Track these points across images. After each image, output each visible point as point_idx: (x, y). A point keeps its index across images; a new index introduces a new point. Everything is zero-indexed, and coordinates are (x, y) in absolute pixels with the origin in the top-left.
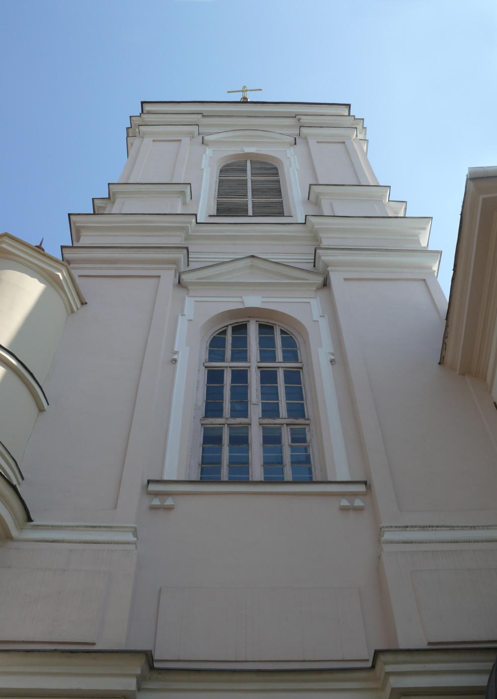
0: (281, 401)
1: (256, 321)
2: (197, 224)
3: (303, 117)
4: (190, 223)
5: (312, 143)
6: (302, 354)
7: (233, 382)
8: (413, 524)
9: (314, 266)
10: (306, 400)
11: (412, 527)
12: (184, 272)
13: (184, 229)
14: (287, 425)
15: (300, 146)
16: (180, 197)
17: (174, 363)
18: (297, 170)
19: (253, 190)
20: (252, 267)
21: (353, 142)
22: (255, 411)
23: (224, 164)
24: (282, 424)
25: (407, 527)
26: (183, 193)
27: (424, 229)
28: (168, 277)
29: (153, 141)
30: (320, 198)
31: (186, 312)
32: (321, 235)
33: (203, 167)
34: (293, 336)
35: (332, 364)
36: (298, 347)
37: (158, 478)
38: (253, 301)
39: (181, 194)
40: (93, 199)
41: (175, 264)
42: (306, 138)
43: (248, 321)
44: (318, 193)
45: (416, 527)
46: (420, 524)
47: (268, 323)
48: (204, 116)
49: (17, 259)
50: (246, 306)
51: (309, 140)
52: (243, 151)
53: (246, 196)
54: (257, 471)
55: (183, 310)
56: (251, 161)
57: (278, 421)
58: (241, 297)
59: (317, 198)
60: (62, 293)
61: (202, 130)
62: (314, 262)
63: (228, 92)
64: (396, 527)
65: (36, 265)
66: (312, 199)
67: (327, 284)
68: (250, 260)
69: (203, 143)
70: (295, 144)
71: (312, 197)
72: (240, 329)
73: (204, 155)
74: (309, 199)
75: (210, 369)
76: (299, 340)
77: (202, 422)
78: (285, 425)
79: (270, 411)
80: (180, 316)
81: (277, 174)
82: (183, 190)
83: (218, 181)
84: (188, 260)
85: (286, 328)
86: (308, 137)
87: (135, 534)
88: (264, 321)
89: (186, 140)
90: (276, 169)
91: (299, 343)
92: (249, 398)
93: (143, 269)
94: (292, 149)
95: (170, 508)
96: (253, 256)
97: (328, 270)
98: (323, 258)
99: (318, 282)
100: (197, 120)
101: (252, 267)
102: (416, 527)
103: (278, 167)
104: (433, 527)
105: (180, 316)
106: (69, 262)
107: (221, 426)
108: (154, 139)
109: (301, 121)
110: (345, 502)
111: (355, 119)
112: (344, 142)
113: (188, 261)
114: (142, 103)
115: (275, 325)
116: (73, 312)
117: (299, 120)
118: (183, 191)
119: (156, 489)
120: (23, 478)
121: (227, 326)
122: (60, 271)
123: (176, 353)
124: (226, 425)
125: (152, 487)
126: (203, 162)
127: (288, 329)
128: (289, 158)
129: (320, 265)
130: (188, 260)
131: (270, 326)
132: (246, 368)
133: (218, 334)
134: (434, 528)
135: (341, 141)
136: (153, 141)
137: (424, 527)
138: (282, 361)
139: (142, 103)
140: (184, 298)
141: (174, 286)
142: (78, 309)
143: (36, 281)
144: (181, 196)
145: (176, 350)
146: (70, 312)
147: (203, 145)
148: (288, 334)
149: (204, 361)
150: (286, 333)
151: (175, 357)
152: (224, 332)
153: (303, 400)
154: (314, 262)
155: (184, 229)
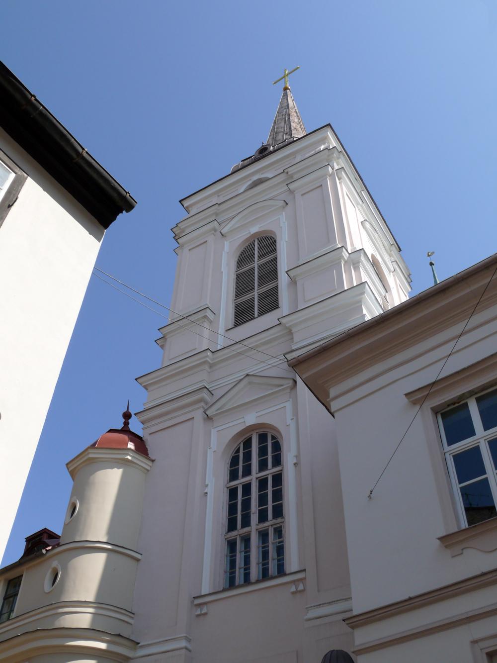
3: (289, 170)
4: (207, 356)
8: (324, 602)
11: (323, 604)
12: (207, 409)
14: (272, 525)
16: (205, 321)
18: (286, 242)
20: (250, 383)
23: (239, 253)
24: (269, 526)
25: (320, 605)
26: (205, 317)
27: (363, 293)
28: (198, 415)
30: (296, 280)
31: (212, 446)
33: (222, 270)
35: (296, 466)
37: (199, 595)
45: (325, 603)
46: (328, 601)
48: (219, 204)
54: (255, 571)
60: (134, 465)
64: (314, 606)
65: (112, 458)
68: (247, 378)
70: (287, 204)
72: (248, 443)
73: (223, 252)
78: (270, 527)
80: (209, 450)
82: (204, 315)
84: (209, 391)
85: (276, 434)
87: (188, 640)
95: (206, 614)
96: (248, 375)
99: (290, 385)
101: (250, 383)
102: (325, 603)
104: (335, 601)
105: (209, 450)
108: (190, 248)
109: (289, 173)
110: (293, 589)
116: (148, 471)
117: (287, 173)
119: (199, 602)
120: (134, 614)
122: (128, 454)
123: (207, 486)
125: (197, 601)
128: (281, 227)
130: (209, 391)
133: (235, 453)
134: (336, 602)
135: (317, 185)
137: (330, 603)
139: (180, 202)
140: (210, 431)
141: (204, 420)
142: (150, 466)
143: (116, 469)
144: (206, 320)
145: (207, 483)
152: (238, 451)
155: (205, 362)
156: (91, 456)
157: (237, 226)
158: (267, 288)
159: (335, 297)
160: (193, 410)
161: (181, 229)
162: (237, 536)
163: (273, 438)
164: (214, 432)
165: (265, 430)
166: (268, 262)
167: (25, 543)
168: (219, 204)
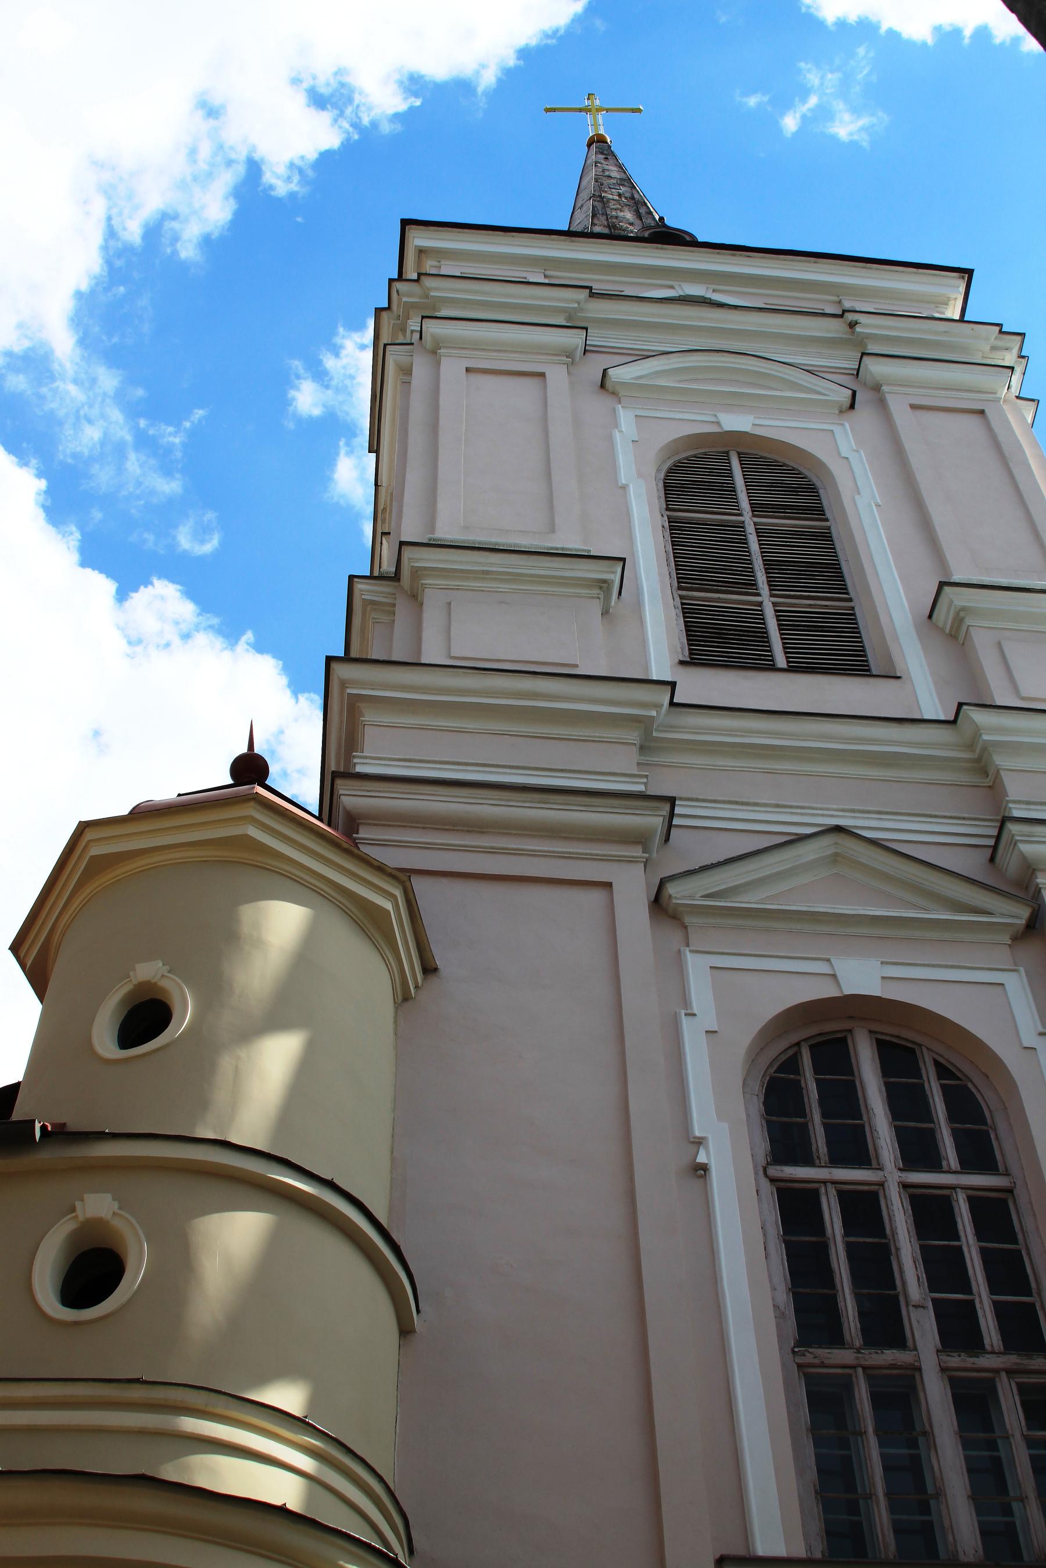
0: (980, 1296)
1: (870, 1032)
2: (673, 709)
5: (898, 406)
6: (1005, 1145)
7: (847, 1233)
9: (992, 860)
10: (1039, 1294)
13: (644, 723)
14: (1010, 1372)
15: (865, 413)
17: (701, 1176)
19: (768, 566)
20: (835, 859)
21: (1005, 407)
22: (923, 1328)
24: (996, 1371)
28: (632, 888)
29: (468, 370)
32: (1001, 761)
34: (970, 1085)
36: (989, 1121)
38: (862, 975)
39: (601, 588)
40: (351, 578)
41: (636, 843)
42: (877, 388)
43: (850, 1031)
44: (963, 609)
47: (898, 1037)
48: (593, 295)
49: (270, 861)
50: (848, 991)
51: (889, 398)
52: (718, 423)
53: (751, 585)
55: (686, 1002)
56: (739, 454)
57: (985, 1361)
58: (828, 960)
59: (959, 620)
61: (596, 339)
62: (995, 848)
63: (548, 110)
66: (946, 619)
67: (1037, 926)
69: (603, 386)
71: (942, 615)
72: (833, 1055)
74: (930, 617)
75: (782, 1184)
76: (987, 1098)
77: (800, 1360)
78: (1003, 1375)
79: (958, 1329)
81: (818, 511)
83: (667, 525)
86: (885, 388)
88: (889, 1030)
89: (557, 375)
90: (812, 489)
91: (991, 1111)
92: (898, 1282)
93: (562, 856)
94: (847, 425)
96: (838, 829)
97: (1037, 884)
98: (1024, 847)
100: (576, 305)
101: (835, 859)
103: (818, 484)
105: (685, 1022)
106: (352, 823)
107: (847, 1371)
109: (858, 329)
111: (1001, 332)
112: (982, 412)
113: (670, 825)
114: (405, 223)
115: (920, 1045)
117: (852, 325)
118: (604, 581)
121: (798, 1044)
123: (699, 1142)
124: (860, 1370)
126: (621, 460)
127: (952, 1060)
129: (1011, 864)
131: (908, 1048)
132: (873, 1188)
136: (468, 370)
138: (959, 1169)
139: (405, 223)
146: (400, 998)
147: (602, 391)
148: (959, 1079)
149: (764, 1163)
150: (951, 1075)
151: (702, 1158)
153: (1030, 1295)
154: (995, 848)
156: (96, 850)
157: (662, 382)
158: (810, 606)
159: (444, 881)
160: (620, 860)
161: (427, 297)
162: (854, 1367)
163: (943, 1071)
164: (697, 968)
165: (918, 1039)
166: (796, 533)
167: (88, 572)
168: (593, 295)
